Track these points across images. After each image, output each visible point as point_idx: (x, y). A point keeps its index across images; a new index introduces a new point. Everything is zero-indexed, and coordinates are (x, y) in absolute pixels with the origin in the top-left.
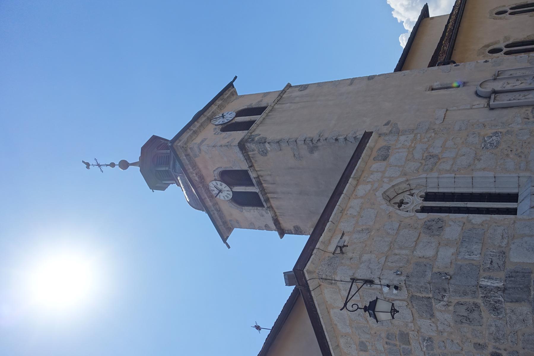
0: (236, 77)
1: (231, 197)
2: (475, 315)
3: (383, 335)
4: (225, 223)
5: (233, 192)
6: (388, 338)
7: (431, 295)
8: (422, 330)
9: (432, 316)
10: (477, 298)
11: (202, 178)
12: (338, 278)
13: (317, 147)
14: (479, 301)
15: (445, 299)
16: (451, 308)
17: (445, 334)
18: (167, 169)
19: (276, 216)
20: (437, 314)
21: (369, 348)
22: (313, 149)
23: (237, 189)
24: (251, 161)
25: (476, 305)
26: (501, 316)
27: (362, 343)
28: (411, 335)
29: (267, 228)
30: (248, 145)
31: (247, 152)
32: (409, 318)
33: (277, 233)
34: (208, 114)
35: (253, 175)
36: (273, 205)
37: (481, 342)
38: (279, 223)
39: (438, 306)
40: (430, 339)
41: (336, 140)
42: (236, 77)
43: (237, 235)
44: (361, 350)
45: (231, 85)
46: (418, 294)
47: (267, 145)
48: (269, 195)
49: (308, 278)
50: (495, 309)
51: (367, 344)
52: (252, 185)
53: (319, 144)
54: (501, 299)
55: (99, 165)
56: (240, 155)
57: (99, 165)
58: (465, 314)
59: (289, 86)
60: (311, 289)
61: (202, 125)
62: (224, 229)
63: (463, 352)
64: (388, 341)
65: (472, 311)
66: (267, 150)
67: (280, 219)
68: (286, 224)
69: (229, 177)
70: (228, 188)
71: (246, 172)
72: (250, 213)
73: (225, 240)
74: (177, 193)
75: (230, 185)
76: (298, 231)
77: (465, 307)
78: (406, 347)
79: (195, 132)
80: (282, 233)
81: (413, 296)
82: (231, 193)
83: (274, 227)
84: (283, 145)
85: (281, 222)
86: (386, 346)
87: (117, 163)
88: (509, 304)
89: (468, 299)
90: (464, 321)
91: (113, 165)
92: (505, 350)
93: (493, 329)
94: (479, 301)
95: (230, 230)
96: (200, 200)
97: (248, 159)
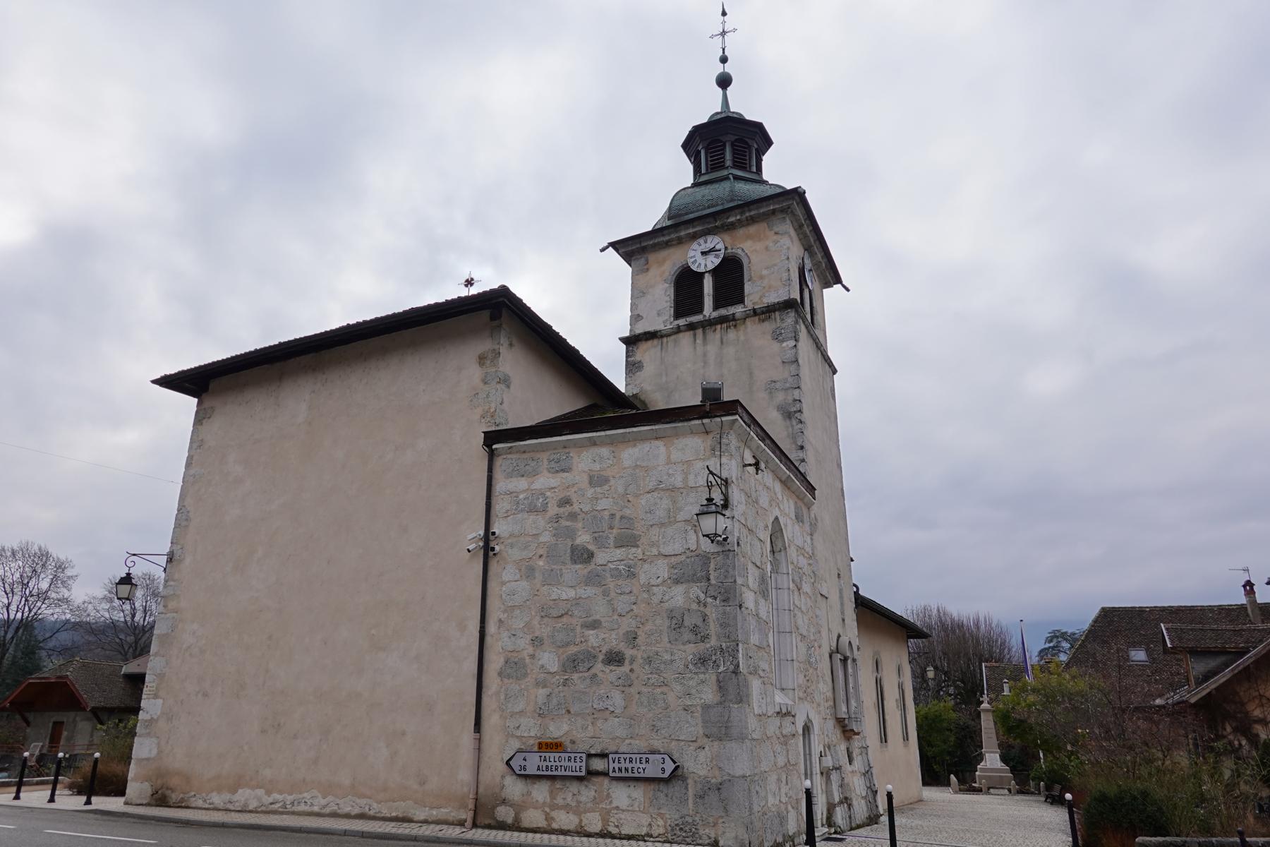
0: (848, 290)
1: (694, 268)
2: (687, 636)
3: (627, 512)
4: (644, 250)
5: (703, 274)
6: (622, 517)
7: (713, 582)
8: (646, 566)
9: (677, 582)
10: (719, 638)
11: (730, 227)
12: (724, 460)
13: (790, 418)
14: (713, 642)
15: (709, 600)
16: (694, 606)
17: (645, 595)
18: (728, 163)
19: (662, 337)
20: (680, 589)
21: (598, 490)
22: (788, 415)
23: (708, 284)
24: (763, 313)
25: (705, 638)
26: (691, 666)
27: (607, 480)
28: (633, 550)
29: (635, 318)
30: (792, 314)
31: (779, 310)
32: (668, 550)
33: (627, 334)
34: (816, 249)
35: (738, 310)
36: (681, 335)
37: (639, 641)
38: (647, 340)
39: (696, 590)
40: (632, 575)
41: (802, 448)
42: (848, 290)
43: (620, 269)
44: (591, 478)
45: (837, 280)
46: (712, 566)
47: (792, 343)
48: (700, 331)
49: (724, 419)
50: (702, 661)
51: (606, 487)
52: (716, 308)
53: (794, 422)
54: (721, 669)
55: (723, 33)
56: (773, 298)
57: (723, 33)
58: (686, 623)
59: (835, 372)
60: (706, 421)
61: (806, 236)
62: (632, 249)
63: (616, 617)
64: (618, 517)
65: (695, 630)
66: (783, 341)
67: (655, 341)
68: (647, 352)
69: (730, 276)
70: (711, 267)
71: (741, 300)
72: (663, 295)
73: (615, 245)
74: (682, 173)
75: (715, 272)
76: (632, 367)
77: (700, 623)
78: (611, 541)
79: (801, 226)
80: (626, 341)
81: (709, 558)
82: (702, 270)
83: (640, 329)
84: (793, 367)
85: (650, 343)
86: (606, 513)
87: (729, 68)
88: (714, 678)
89: (713, 628)
90: (674, 621)
91: (724, 60)
92: (631, 670)
93: (667, 657)
94: (713, 642)
95: (628, 257)
96: (682, 222)
97: (767, 312)
